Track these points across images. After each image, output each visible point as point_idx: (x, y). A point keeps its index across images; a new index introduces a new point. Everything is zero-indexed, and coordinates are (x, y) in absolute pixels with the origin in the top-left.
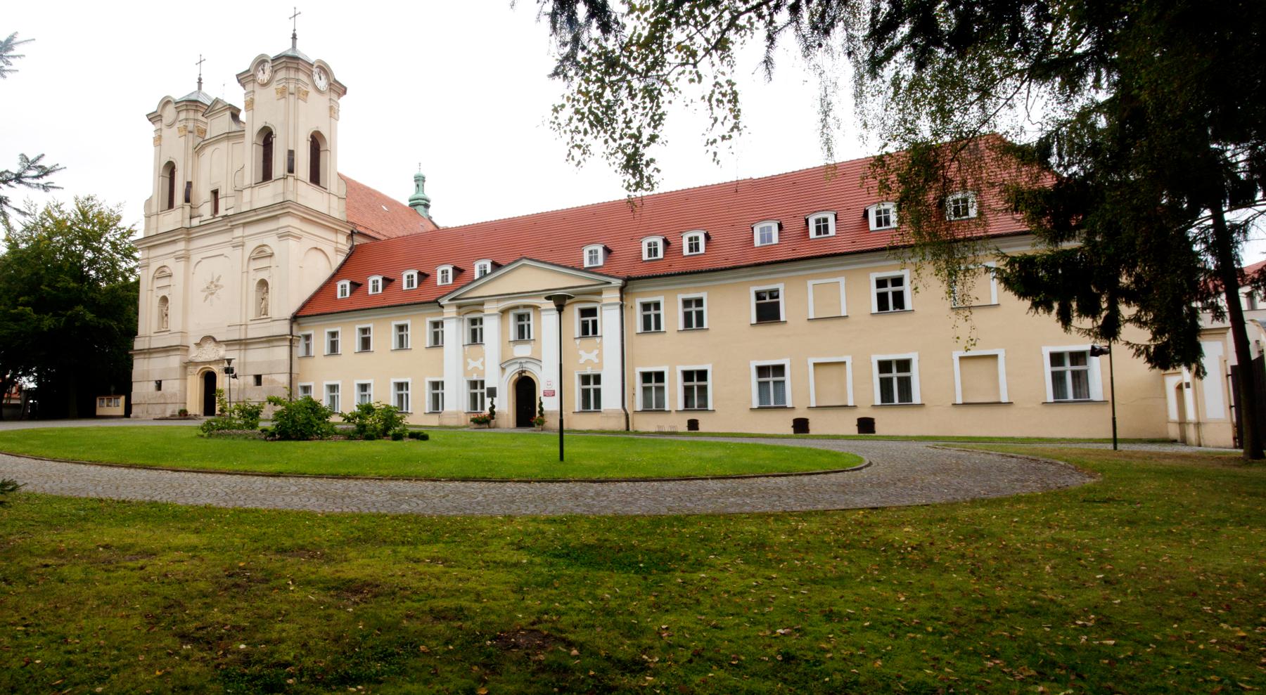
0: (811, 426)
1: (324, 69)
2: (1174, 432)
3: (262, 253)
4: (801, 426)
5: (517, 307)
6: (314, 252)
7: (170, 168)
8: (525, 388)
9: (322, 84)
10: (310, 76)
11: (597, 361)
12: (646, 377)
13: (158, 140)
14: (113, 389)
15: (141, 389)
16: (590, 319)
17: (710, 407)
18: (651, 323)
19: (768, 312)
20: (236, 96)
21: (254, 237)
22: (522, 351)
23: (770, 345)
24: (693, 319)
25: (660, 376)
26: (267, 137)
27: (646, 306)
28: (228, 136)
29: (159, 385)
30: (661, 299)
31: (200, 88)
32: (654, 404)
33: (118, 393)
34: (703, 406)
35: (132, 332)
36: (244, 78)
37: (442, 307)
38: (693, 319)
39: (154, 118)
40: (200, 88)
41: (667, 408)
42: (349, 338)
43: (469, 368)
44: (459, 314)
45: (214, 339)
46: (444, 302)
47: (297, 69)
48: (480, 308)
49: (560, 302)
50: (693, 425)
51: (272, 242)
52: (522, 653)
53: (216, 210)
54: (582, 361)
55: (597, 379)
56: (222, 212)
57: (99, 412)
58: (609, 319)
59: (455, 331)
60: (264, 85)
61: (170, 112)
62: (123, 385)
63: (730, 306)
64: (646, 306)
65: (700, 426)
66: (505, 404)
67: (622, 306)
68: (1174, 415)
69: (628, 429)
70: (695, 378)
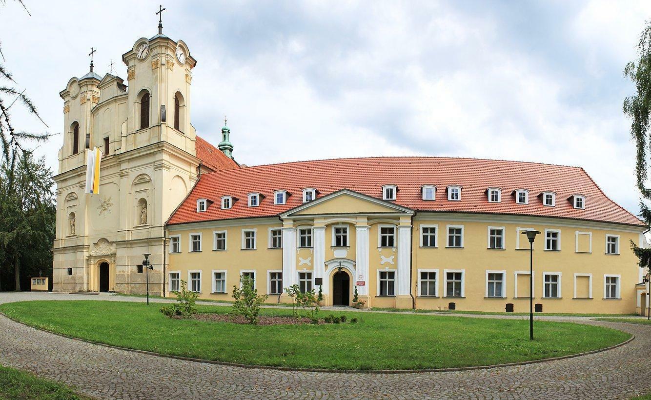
0: (515, 308)
1: (184, 47)
2: (639, 311)
3: (142, 179)
4: (510, 308)
5: (337, 223)
6: (177, 178)
7: (76, 126)
8: (341, 281)
9: (182, 59)
10: (174, 52)
11: (392, 263)
12: (424, 275)
13: (66, 110)
14: (41, 273)
15: (59, 273)
16: (388, 235)
17: (463, 295)
18: (429, 241)
19: (496, 243)
20: (121, 71)
21: (133, 170)
22: (341, 253)
23: (495, 262)
24: (455, 242)
25: (433, 275)
26: (145, 98)
27: (425, 230)
28: (115, 99)
29: (70, 272)
30: (436, 226)
31: (91, 70)
32: (428, 292)
33: (44, 276)
34: (458, 295)
35: (53, 238)
36: (125, 59)
37: (282, 220)
38: (455, 242)
39: (63, 94)
40: (91, 70)
41: (437, 295)
42: (209, 241)
43: (300, 264)
44: (294, 225)
45: (107, 240)
46: (284, 217)
47: (167, 47)
48: (310, 222)
49: (371, 218)
50: (452, 306)
51: (149, 171)
52: (317, 391)
53: (107, 151)
54: (382, 263)
55: (392, 275)
56: (111, 153)
57: (33, 287)
58: (403, 237)
59: (291, 238)
60: (142, 60)
61: (74, 90)
62: (47, 271)
63: (475, 237)
64: (425, 230)
65: (456, 307)
66: (327, 289)
67: (412, 228)
68: (639, 305)
69: (414, 308)
70: (454, 277)
